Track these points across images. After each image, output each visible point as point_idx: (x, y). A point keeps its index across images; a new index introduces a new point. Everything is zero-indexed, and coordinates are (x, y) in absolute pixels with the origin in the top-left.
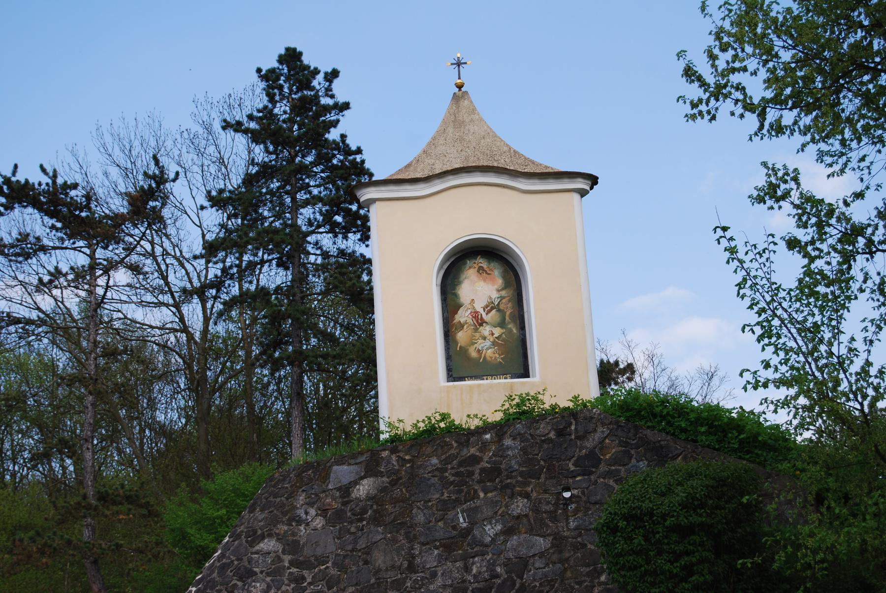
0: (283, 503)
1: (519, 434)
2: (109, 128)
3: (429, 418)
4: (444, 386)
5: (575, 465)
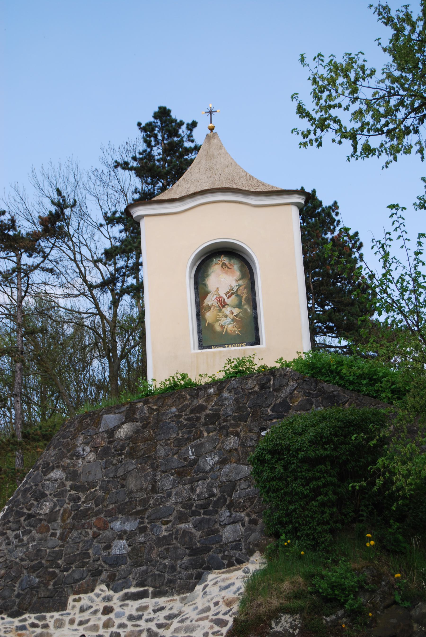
0: (68, 443)
1: (234, 388)
2: (41, 169)
3: (173, 378)
4: (194, 353)
5: (272, 410)
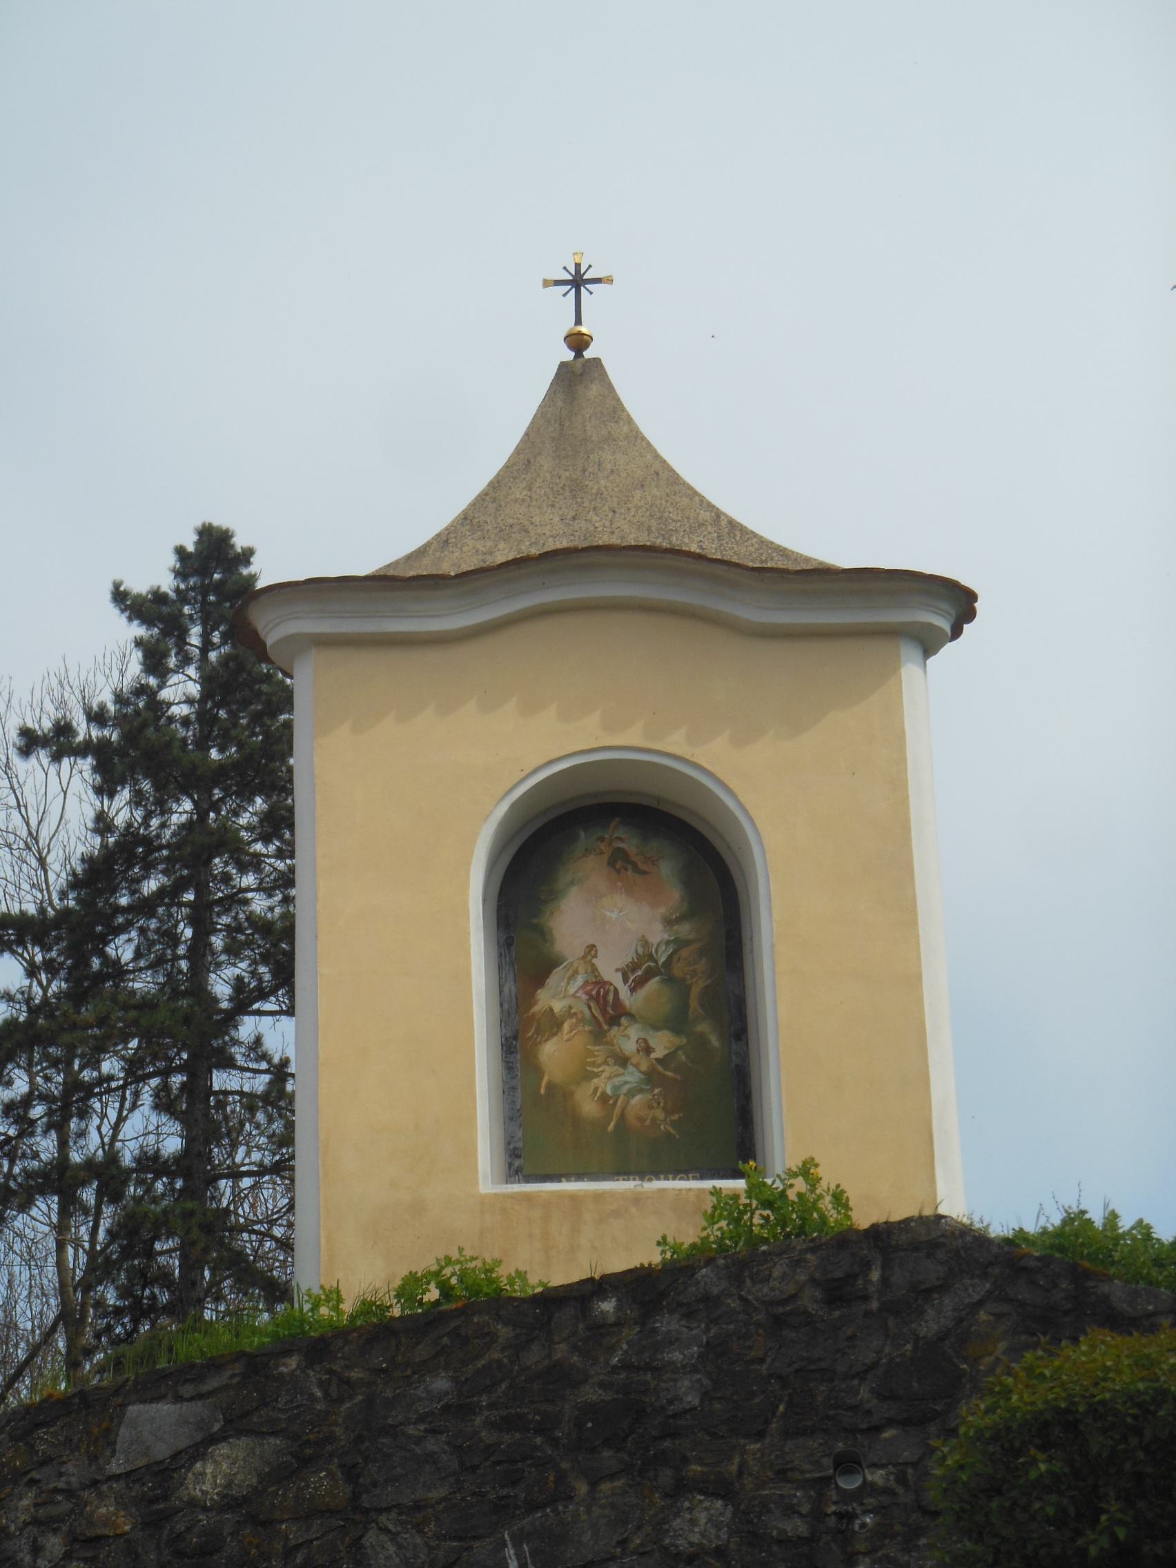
1: (706, 1299)
